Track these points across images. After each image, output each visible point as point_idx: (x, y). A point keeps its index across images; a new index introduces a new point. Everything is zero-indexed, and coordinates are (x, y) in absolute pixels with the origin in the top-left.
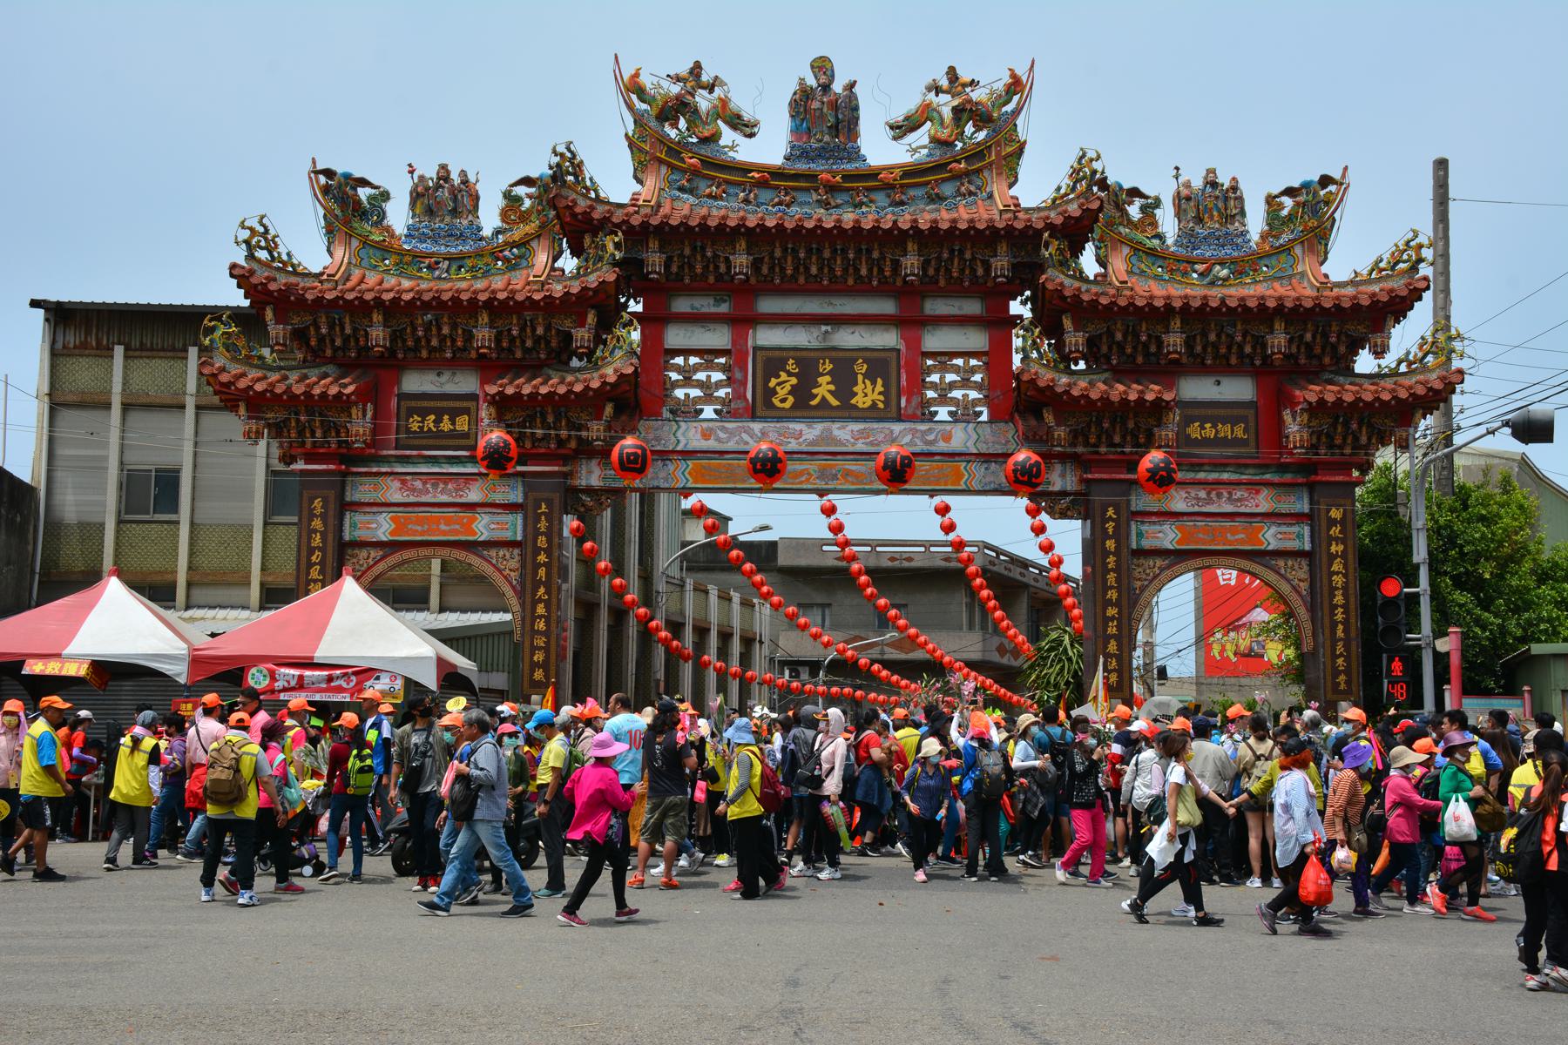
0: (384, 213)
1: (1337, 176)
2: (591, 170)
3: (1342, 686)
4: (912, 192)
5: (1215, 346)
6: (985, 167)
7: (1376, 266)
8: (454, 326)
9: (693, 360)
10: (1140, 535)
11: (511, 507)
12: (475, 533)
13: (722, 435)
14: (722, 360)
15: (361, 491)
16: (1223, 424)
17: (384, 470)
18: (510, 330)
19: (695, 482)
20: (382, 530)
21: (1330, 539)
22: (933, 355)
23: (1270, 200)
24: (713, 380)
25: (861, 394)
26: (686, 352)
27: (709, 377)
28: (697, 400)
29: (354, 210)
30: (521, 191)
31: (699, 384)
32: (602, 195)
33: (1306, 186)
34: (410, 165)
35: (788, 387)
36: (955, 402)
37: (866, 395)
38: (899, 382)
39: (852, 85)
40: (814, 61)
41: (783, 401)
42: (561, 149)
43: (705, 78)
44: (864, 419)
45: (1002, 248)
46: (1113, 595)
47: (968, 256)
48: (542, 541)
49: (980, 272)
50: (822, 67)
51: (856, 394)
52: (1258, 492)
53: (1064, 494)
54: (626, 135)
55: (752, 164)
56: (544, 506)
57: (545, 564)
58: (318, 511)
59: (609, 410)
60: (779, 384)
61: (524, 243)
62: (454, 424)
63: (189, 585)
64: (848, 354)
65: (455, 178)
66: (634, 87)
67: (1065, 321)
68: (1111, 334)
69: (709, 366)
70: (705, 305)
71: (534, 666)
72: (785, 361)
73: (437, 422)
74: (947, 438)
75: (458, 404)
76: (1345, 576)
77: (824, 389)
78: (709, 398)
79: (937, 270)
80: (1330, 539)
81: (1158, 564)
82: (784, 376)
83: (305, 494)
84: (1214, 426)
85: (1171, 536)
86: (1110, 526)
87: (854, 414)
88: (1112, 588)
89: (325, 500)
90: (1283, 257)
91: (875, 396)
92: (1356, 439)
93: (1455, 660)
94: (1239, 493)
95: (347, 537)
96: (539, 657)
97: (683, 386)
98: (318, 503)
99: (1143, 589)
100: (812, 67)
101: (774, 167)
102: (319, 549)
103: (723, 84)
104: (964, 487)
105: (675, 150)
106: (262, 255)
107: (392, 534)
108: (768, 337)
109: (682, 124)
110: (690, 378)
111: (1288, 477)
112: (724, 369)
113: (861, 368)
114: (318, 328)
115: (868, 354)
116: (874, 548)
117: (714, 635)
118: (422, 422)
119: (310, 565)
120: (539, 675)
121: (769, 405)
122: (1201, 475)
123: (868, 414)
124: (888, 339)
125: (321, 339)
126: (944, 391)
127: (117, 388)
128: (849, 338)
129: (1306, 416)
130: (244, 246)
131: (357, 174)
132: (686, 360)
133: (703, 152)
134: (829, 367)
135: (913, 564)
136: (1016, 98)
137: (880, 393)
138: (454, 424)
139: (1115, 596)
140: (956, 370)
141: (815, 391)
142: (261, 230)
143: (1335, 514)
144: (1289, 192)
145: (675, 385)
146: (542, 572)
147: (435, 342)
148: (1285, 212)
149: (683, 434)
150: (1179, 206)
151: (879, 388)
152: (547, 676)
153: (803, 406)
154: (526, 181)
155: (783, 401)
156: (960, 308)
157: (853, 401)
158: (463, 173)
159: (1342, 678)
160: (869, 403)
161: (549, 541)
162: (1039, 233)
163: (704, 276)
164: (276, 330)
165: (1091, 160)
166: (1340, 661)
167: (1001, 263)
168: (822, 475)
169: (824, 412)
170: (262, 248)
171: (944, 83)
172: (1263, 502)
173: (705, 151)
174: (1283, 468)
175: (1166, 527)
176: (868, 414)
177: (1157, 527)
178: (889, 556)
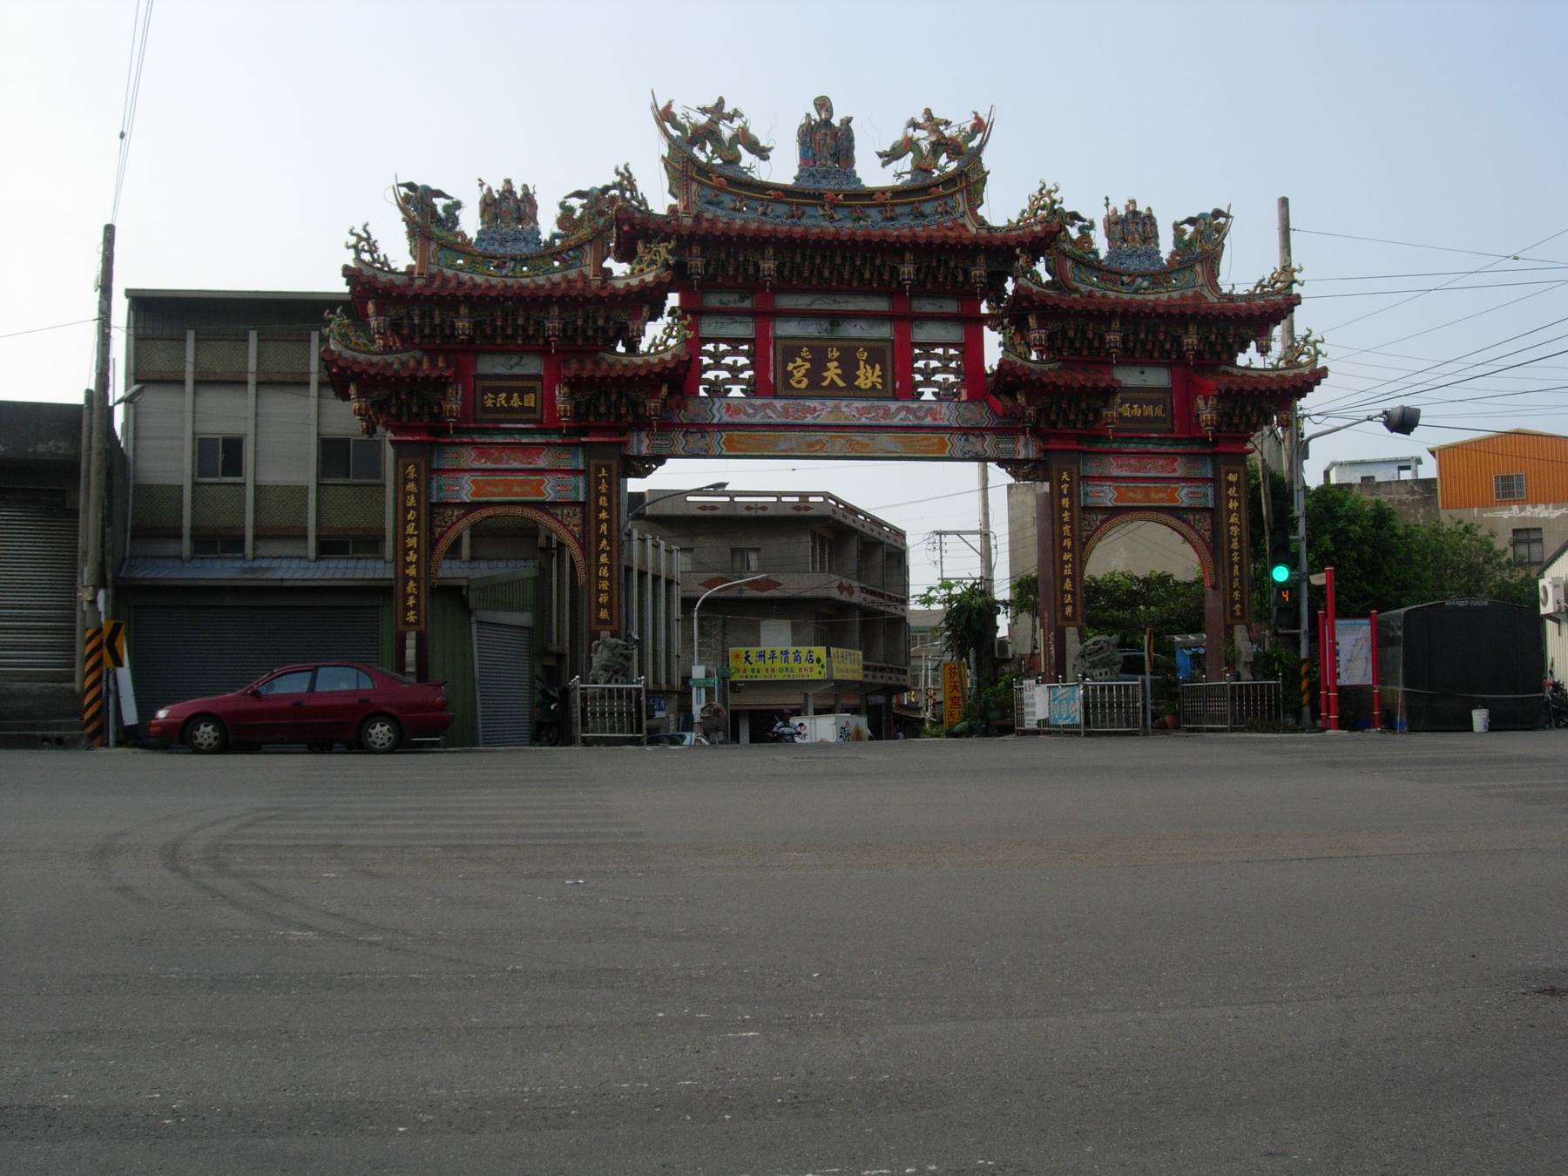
0: (457, 218)
2: (642, 187)
3: (1238, 613)
4: (899, 210)
5: (1143, 343)
6: (957, 191)
7: (1260, 284)
9: (723, 347)
11: (574, 472)
14: (746, 347)
17: (465, 440)
18: (575, 321)
19: (728, 451)
20: (465, 492)
21: (1229, 498)
22: (919, 345)
23: (1177, 227)
24: (739, 364)
25: (862, 377)
26: (717, 340)
27: (735, 362)
28: (726, 381)
29: (432, 218)
30: (576, 203)
33: (1203, 216)
34: (480, 180)
35: (803, 371)
36: (936, 384)
37: (867, 378)
38: (775, 353)
39: (849, 120)
40: (816, 99)
41: (799, 382)
42: (622, 170)
43: (728, 109)
44: (867, 398)
45: (981, 260)
46: (1068, 543)
47: (952, 265)
48: (603, 501)
49: (961, 278)
50: (823, 104)
51: (859, 377)
52: (1174, 460)
53: (1026, 461)
54: (663, 157)
56: (603, 471)
57: (606, 520)
58: (412, 476)
59: (664, 390)
60: (795, 368)
61: (579, 247)
62: (522, 401)
63: (256, 538)
64: (851, 344)
66: (665, 116)
67: (1030, 320)
70: (731, 300)
72: (800, 348)
73: (508, 399)
75: (526, 384)
76: (1240, 526)
77: (832, 372)
78: (735, 380)
79: (926, 276)
80: (1229, 498)
81: (1099, 518)
82: (799, 362)
83: (400, 462)
84: (1140, 407)
86: (1065, 487)
87: (858, 393)
88: (1067, 537)
89: (417, 466)
90: (1188, 273)
91: (875, 379)
92: (1249, 419)
96: (603, 599)
97: (715, 369)
100: (815, 104)
102: (413, 507)
103: (741, 116)
104: (948, 455)
105: (705, 170)
109: (709, 148)
110: (719, 362)
111: (1196, 448)
114: (494, 320)
116: (779, 499)
117: (650, 577)
118: (495, 399)
120: (604, 614)
123: (869, 394)
124: (884, 331)
126: (928, 373)
127: (190, 368)
128: (853, 330)
129: (1215, 401)
131: (434, 187)
133: (727, 172)
134: (836, 354)
135: (767, 513)
136: (979, 136)
137: (878, 377)
138: (522, 401)
139: (1069, 544)
141: (825, 374)
142: (365, 235)
143: (1232, 478)
144: (1191, 221)
145: (708, 368)
146: (604, 527)
147: (510, 331)
148: (1186, 237)
149: (718, 410)
150: (1109, 229)
151: (878, 371)
152: (611, 615)
153: (816, 388)
154: (579, 194)
155: (799, 382)
156: (941, 307)
157: (857, 383)
158: (525, 187)
159: (1238, 606)
161: (609, 501)
162: (1012, 249)
163: (735, 277)
165: (1050, 192)
166: (1236, 594)
167: (979, 272)
169: (833, 392)
170: (366, 251)
172: (1180, 469)
173: (729, 171)
174: (1193, 441)
176: (869, 394)
177: (1099, 488)
178: (746, 505)
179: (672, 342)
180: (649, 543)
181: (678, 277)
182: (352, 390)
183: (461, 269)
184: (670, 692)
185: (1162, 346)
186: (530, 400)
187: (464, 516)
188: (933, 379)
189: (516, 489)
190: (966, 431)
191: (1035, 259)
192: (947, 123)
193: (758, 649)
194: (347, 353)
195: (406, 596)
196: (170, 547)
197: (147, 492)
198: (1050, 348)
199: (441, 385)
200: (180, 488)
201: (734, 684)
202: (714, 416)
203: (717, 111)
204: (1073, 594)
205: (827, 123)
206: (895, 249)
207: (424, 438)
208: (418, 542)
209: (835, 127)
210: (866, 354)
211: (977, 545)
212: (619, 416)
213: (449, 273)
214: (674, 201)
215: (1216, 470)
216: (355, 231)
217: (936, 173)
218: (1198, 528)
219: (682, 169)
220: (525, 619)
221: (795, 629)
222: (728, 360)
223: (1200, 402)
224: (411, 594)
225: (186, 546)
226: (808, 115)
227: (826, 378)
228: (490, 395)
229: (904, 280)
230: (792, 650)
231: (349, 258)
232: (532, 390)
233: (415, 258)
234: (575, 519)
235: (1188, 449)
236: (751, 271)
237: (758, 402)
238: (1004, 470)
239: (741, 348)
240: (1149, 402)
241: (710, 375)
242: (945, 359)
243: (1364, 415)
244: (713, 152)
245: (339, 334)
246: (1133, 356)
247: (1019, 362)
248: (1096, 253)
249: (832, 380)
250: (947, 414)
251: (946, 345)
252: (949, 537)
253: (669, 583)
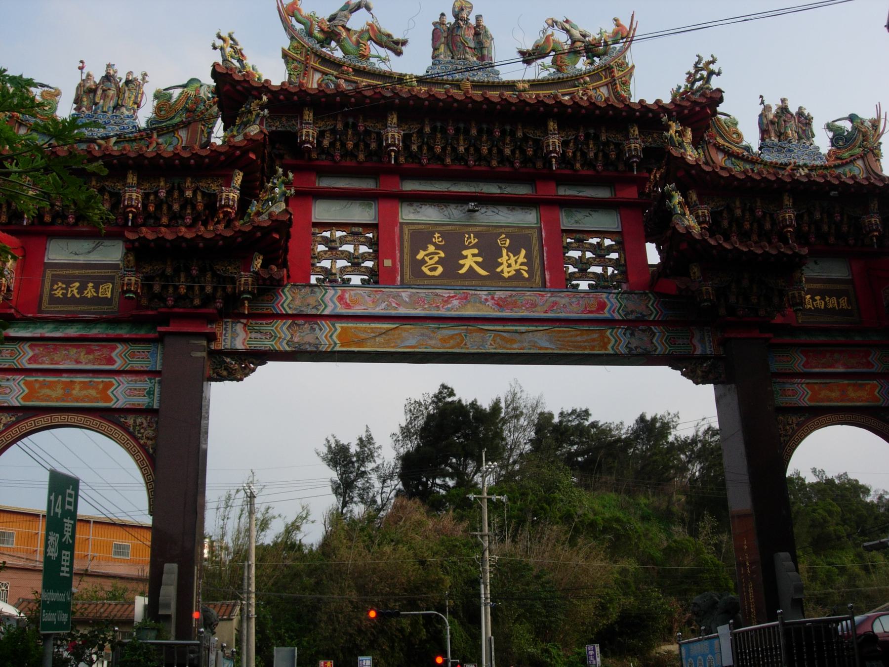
12: (109, 399)
16: (830, 297)
22: (569, 232)
31: (348, 256)
41: (433, 269)
51: (502, 264)
53: (703, 358)
62: (97, 292)
77: (470, 260)
82: (431, 248)
84: (823, 299)
112: (370, 243)
115: (511, 230)
134: (474, 241)
138: (97, 292)
149: (331, 300)
151: (522, 258)
188: (589, 271)
190: (631, 324)
210: (508, 241)
226: (443, 15)
227: (463, 266)
228: (60, 284)
238: (679, 372)
239: (367, 235)
240: (831, 293)
242: (600, 252)
249: (471, 267)
251: (602, 234)
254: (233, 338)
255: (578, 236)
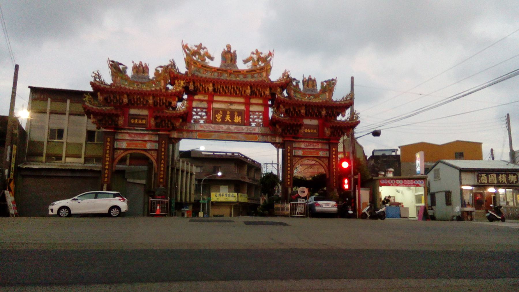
1: (335, 78)
3: (335, 185)
7: (343, 98)
8: (144, 99)
9: (199, 110)
10: (295, 152)
12: (146, 147)
13: (205, 127)
15: (119, 137)
23: (322, 83)
26: (197, 108)
28: (199, 119)
30: (160, 69)
31: (200, 115)
32: (180, 71)
35: (220, 117)
36: (256, 122)
41: (219, 120)
42: (171, 60)
43: (203, 46)
53: (279, 143)
54: (185, 59)
55: (213, 67)
62: (142, 121)
63: (66, 157)
65: (144, 65)
68: (110, 97)
69: (202, 111)
71: (160, 178)
74: (255, 130)
77: (228, 118)
78: (202, 118)
85: (301, 153)
93: (359, 180)
94: (315, 144)
95: (115, 147)
98: (109, 139)
99: (295, 164)
100: (227, 46)
101: (217, 68)
106: (98, 80)
107: (127, 146)
108: (216, 106)
110: (198, 114)
111: (325, 141)
112: (205, 112)
113: (236, 114)
117: (185, 172)
119: (106, 153)
120: (161, 180)
121: (215, 120)
122: (307, 140)
125: (111, 100)
130: (93, 78)
131: (120, 62)
132: (197, 110)
135: (223, 157)
140: (256, 115)
142: (97, 74)
144: (326, 81)
145: (194, 115)
148: (325, 85)
153: (223, 122)
154: (161, 67)
155: (219, 120)
158: (146, 64)
160: (238, 121)
164: (100, 98)
165: (288, 72)
166: (334, 180)
168: (228, 137)
169: (228, 123)
171: (255, 52)
172: (320, 146)
173: (203, 63)
174: (324, 139)
175: (300, 151)
177: (298, 151)
179: (183, 107)
180: (185, 163)
181: (186, 90)
182: (92, 116)
183: (126, 85)
184: (190, 203)
185: (316, 114)
186: (144, 122)
187: (124, 152)
189: (139, 146)
190: (263, 135)
191: (283, 90)
192: (261, 53)
193: (219, 193)
194: (90, 106)
195: (105, 174)
196: (39, 159)
197: (33, 143)
198: (287, 113)
199: (117, 116)
200: (43, 143)
201: (212, 203)
202: (195, 128)
203: (200, 47)
204: (290, 178)
205: (229, 52)
206: (244, 84)
207: (112, 130)
208: (109, 159)
209: (231, 53)
211: (276, 167)
212: (168, 127)
213: (123, 86)
214: (187, 70)
215: (329, 147)
216: (95, 72)
217: (258, 66)
218: (325, 162)
219: (189, 63)
220: (143, 182)
221: (229, 188)
222: (200, 113)
223: (326, 129)
224: (106, 173)
225: (44, 158)
229: (247, 94)
230: (228, 193)
231: (92, 80)
232: (144, 119)
233: (113, 81)
234: (154, 154)
235: (322, 141)
236: (207, 90)
237: (207, 125)
241: (195, 117)
243: (367, 133)
244: (198, 58)
245: (88, 101)
246: (309, 115)
247: (277, 117)
248: (300, 89)
250: (257, 130)
252: (269, 165)
253: (191, 174)
254: (174, 135)
255: (253, 112)
